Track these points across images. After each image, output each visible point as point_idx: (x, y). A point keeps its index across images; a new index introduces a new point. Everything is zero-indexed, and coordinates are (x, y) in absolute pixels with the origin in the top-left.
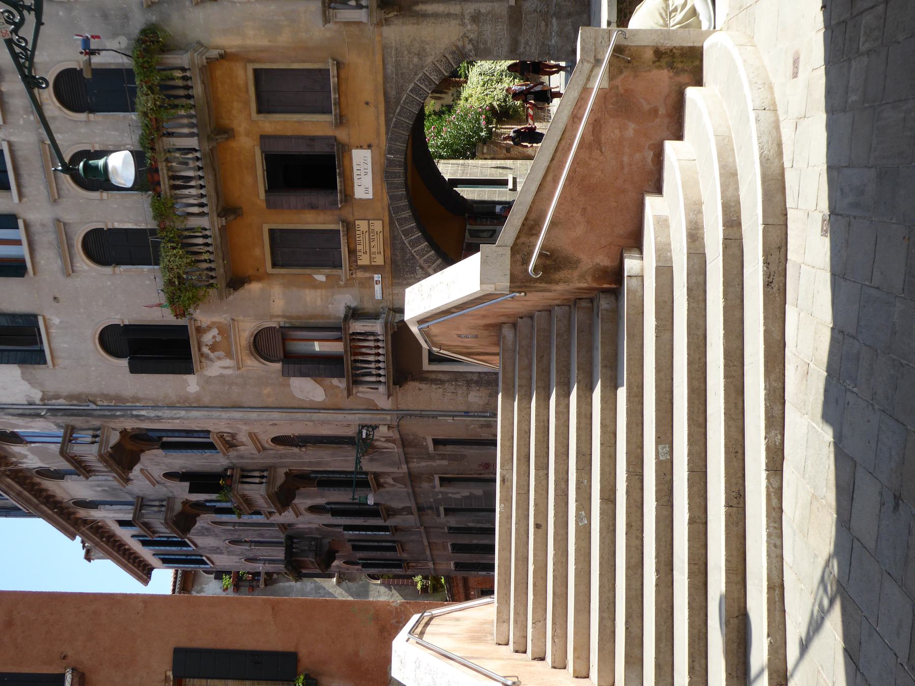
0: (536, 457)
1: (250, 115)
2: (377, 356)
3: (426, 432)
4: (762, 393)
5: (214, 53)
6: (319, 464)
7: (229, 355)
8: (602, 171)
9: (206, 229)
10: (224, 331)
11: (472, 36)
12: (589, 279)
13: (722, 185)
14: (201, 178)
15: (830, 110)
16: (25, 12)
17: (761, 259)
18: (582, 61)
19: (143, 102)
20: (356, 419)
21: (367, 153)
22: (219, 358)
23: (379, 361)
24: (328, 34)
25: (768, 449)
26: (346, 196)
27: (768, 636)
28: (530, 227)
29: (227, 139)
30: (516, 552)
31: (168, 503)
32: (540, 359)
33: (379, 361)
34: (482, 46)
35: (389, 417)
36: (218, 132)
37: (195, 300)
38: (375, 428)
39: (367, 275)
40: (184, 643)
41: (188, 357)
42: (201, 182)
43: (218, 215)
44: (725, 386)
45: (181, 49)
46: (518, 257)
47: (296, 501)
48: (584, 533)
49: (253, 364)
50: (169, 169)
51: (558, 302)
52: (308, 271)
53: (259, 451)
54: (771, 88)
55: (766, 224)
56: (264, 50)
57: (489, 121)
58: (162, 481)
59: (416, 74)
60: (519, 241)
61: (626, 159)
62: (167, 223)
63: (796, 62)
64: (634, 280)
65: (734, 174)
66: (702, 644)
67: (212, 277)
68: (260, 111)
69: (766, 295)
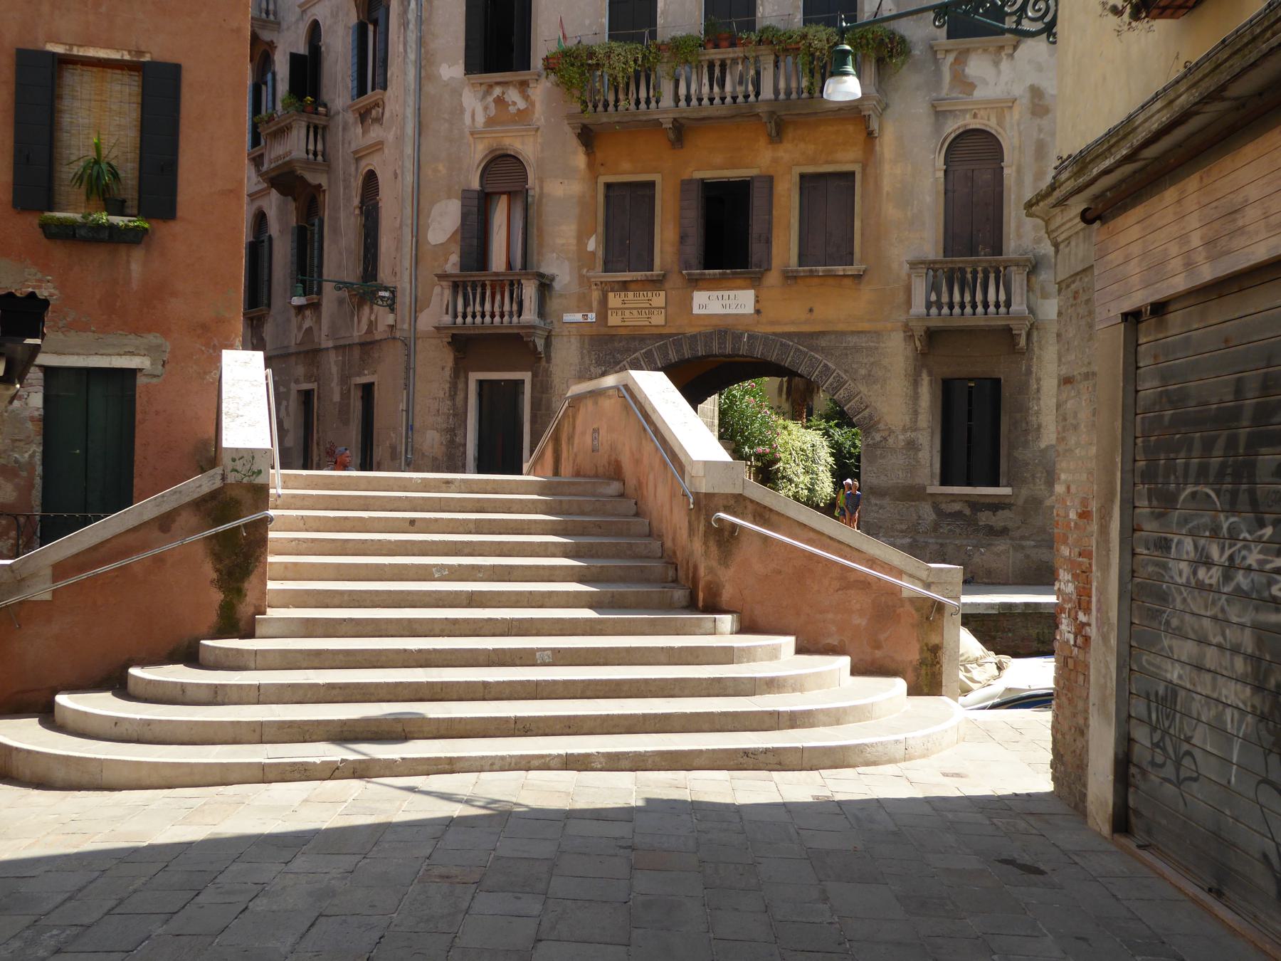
0: (490, 520)
1: (798, 164)
2: (491, 315)
3: (383, 375)
4: (642, 749)
5: (874, 125)
6: (335, 230)
7: (490, 122)
8: (819, 591)
9: (657, 102)
10: (523, 117)
11: (891, 441)
12: (709, 578)
13: (828, 709)
14: (723, 99)
15: (928, 801)
16: (1015, 18)
17: (769, 746)
18: (930, 569)
19: (818, 35)
20: (404, 284)
21: (749, 309)
22: (486, 108)
23: (483, 316)
24: (895, 266)
25: (588, 755)
26: (697, 280)
27: (403, 759)
28: (763, 514)
29: (770, 135)
30: (374, 497)
31: (272, 22)
32: (598, 525)
33: (483, 316)
34: (879, 452)
35: (406, 326)
36: (779, 124)
37: (566, 84)
38: (392, 308)
39: (595, 304)
40: (187, 78)
41: (487, 70)
42: (717, 101)
43: (675, 119)
44: (635, 715)
45: (880, 82)
46: (732, 502)
47: (274, 191)
48: (424, 574)
49: (478, 153)
50: (734, 61)
51: (669, 544)
52: (600, 229)
53: (355, 152)
54: (924, 756)
55: (803, 749)
56: (878, 188)
57: (759, 457)
58: (306, 18)
59: (846, 371)
60: (749, 504)
61: (830, 616)
62: (666, 55)
63: (958, 775)
64: (711, 625)
65: (838, 722)
66: (358, 697)
67: (595, 107)
68: (803, 177)
69: (736, 751)
